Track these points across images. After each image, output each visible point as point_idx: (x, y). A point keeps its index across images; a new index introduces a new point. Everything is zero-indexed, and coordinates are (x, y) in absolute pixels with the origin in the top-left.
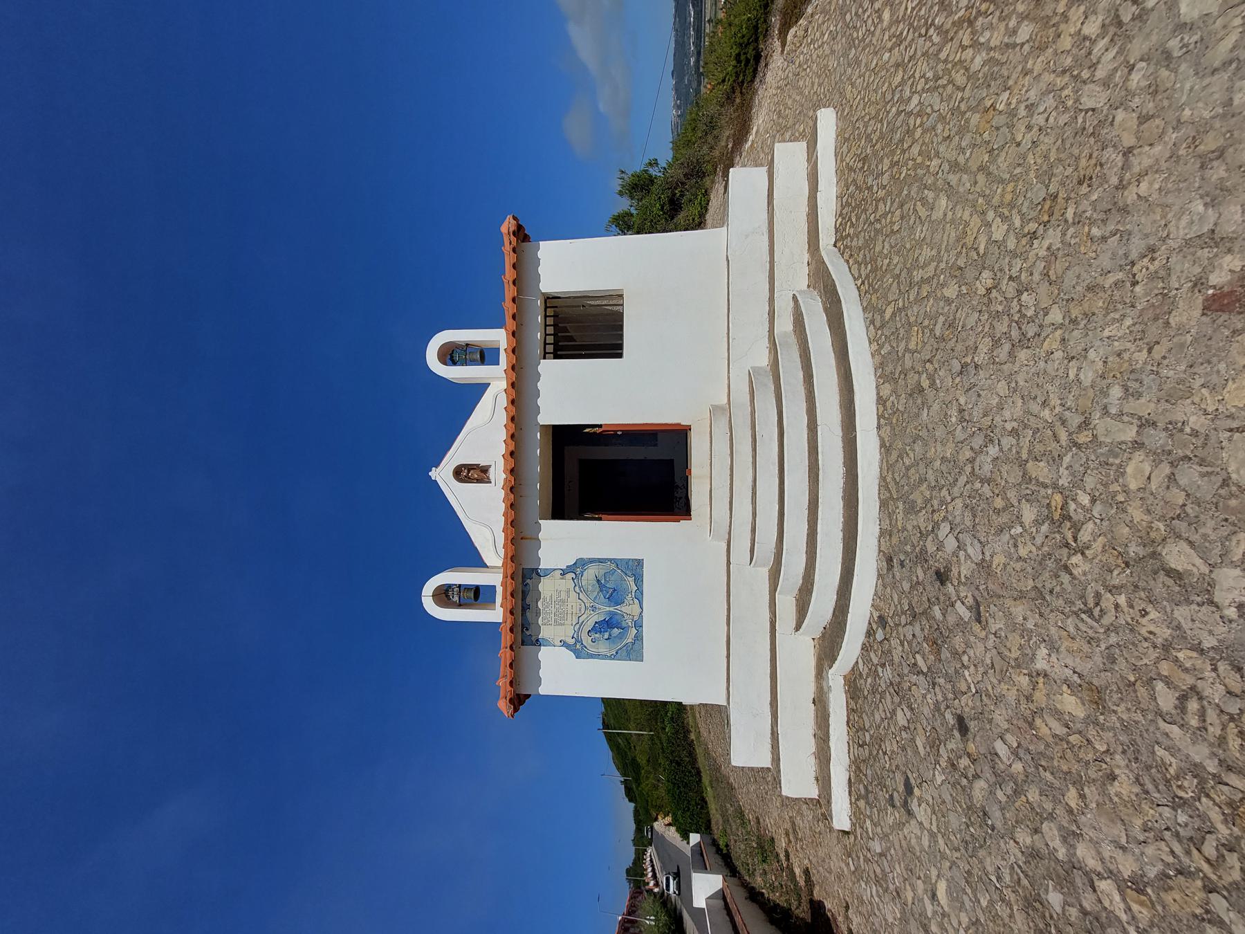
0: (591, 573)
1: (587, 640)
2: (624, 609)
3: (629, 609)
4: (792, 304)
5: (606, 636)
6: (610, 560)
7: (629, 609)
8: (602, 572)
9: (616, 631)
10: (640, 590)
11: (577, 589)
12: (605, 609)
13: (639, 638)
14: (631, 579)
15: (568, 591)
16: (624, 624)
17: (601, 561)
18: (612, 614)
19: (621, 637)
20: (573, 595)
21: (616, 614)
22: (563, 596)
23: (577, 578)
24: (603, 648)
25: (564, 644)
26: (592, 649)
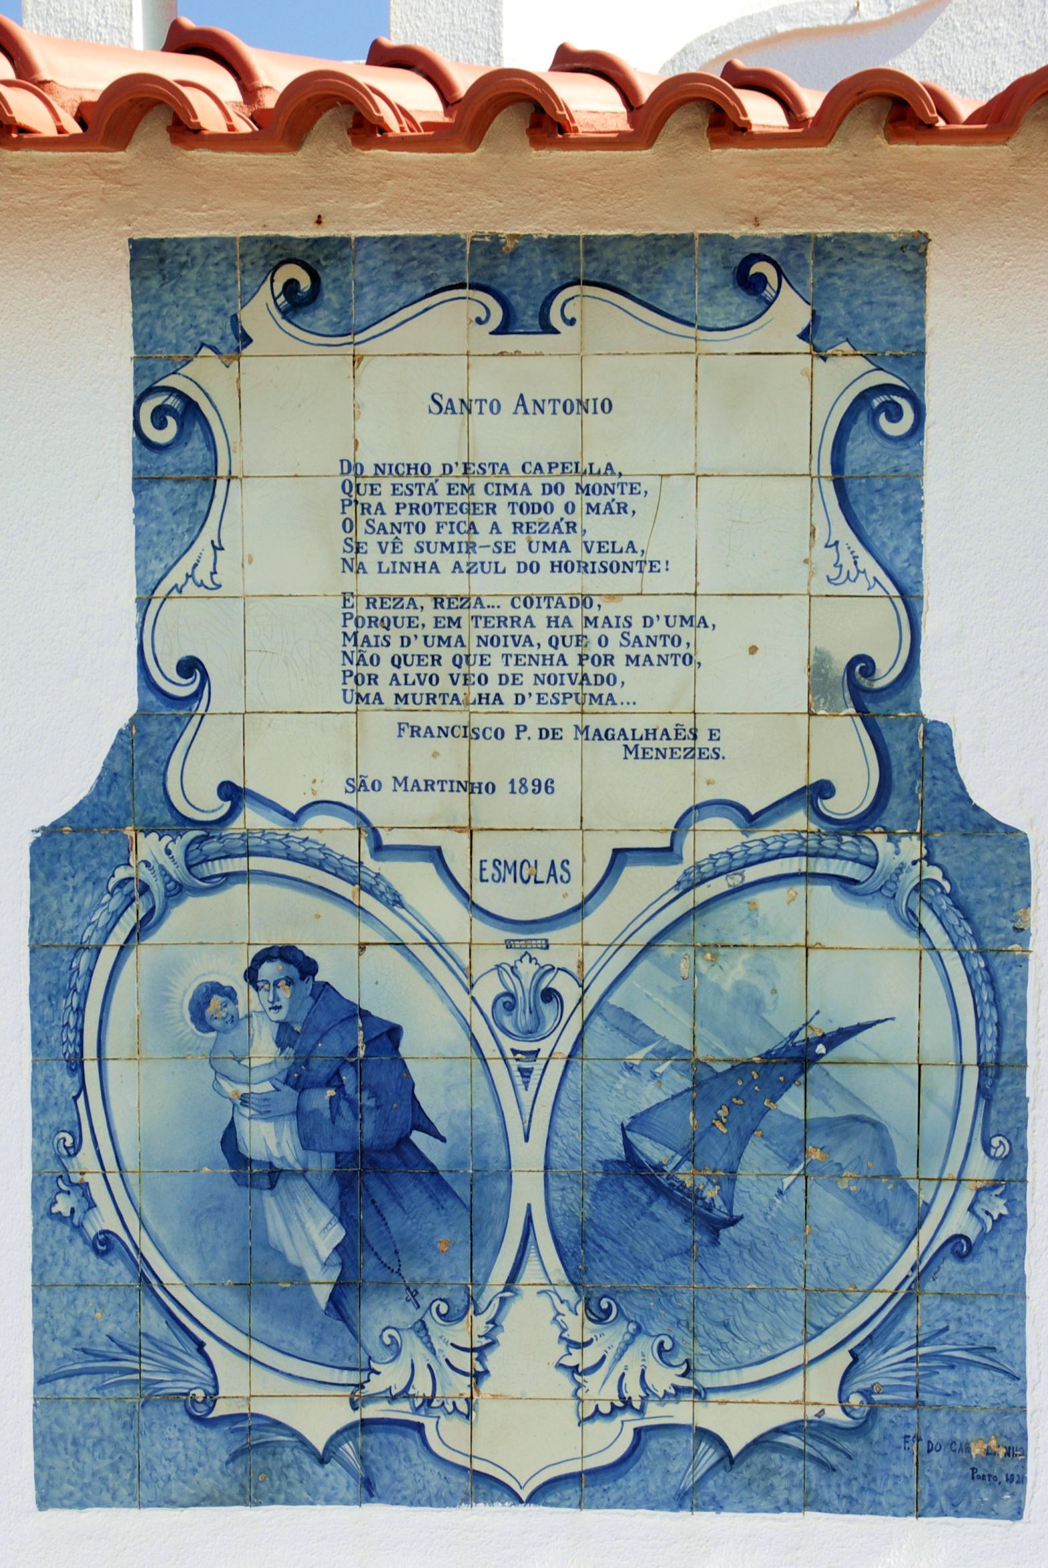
0: (865, 970)
1: (213, 935)
2: (535, 1322)
3: (533, 1371)
4: (525, 1210)
5: (267, 1139)
6: (1009, 1182)
7: (533, 1371)
8: (889, 1097)
9: (310, 1234)
10: (729, 1476)
11: (716, 838)
12: (509, 1118)
13: (259, 1461)
14: (819, 1392)
15: (689, 742)
16: (383, 1316)
17: (998, 1073)
18: (470, 1195)
19: (259, 1280)
20: (647, 798)
21: (480, 1236)
22: (647, 694)
23: (823, 838)
24: (149, 1098)
25: (172, 700)
26: (140, 992)
